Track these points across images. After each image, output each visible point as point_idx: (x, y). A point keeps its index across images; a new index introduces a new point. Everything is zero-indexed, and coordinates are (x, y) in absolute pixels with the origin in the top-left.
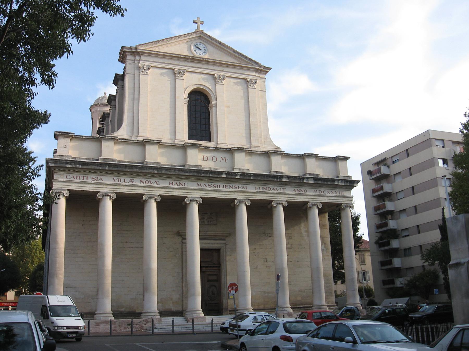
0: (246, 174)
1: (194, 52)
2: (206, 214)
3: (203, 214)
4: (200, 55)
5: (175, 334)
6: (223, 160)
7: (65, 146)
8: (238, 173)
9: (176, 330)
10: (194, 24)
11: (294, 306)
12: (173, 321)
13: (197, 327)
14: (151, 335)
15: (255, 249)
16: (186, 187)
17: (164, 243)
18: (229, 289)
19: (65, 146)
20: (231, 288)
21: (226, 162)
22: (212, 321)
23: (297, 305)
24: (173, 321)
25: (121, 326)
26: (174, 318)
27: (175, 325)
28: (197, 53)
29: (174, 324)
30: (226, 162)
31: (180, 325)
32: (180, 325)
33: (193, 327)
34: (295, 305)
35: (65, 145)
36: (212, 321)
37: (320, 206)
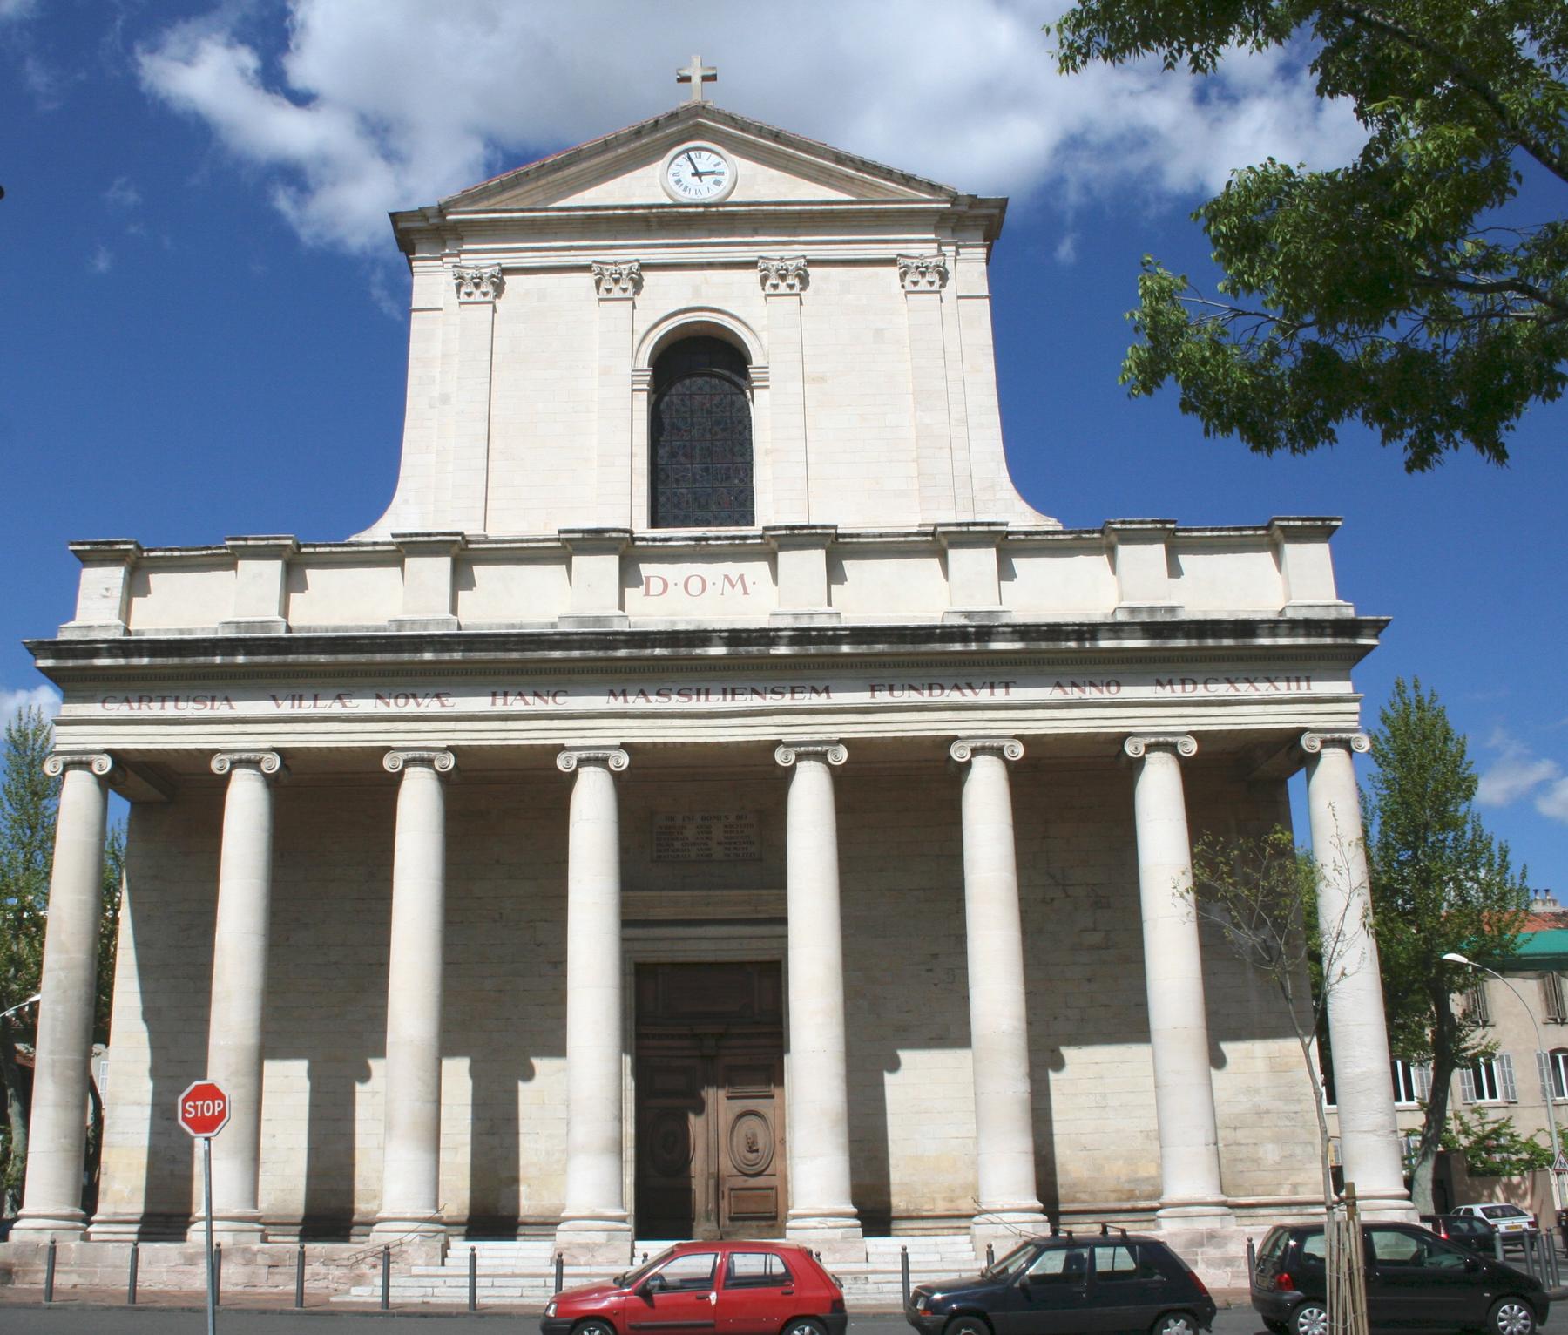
0: (814, 633)
1: (676, 187)
2: (719, 818)
3: (704, 818)
4: (701, 197)
5: (482, 1316)
6: (733, 586)
7: (104, 593)
8: (781, 633)
9: (486, 1296)
10: (681, 84)
11: (1120, 1200)
12: (473, 1258)
13: (493, 1286)
14: (465, 1315)
15: (935, 956)
16: (560, 708)
17: (539, 946)
18: (185, 1111)
19: (104, 593)
20: (195, 1107)
21: (746, 593)
22: (905, 1257)
23: (1138, 1199)
24: (473, 1258)
25: (276, 1270)
26: (479, 1245)
27: (481, 1276)
28: (685, 190)
29: (910, 1268)
30: (746, 593)
31: (514, 1276)
32: (514, 1276)
33: (473, 1288)
34: (1128, 1199)
35: (107, 589)
36: (905, 1257)
37: (1190, 748)
